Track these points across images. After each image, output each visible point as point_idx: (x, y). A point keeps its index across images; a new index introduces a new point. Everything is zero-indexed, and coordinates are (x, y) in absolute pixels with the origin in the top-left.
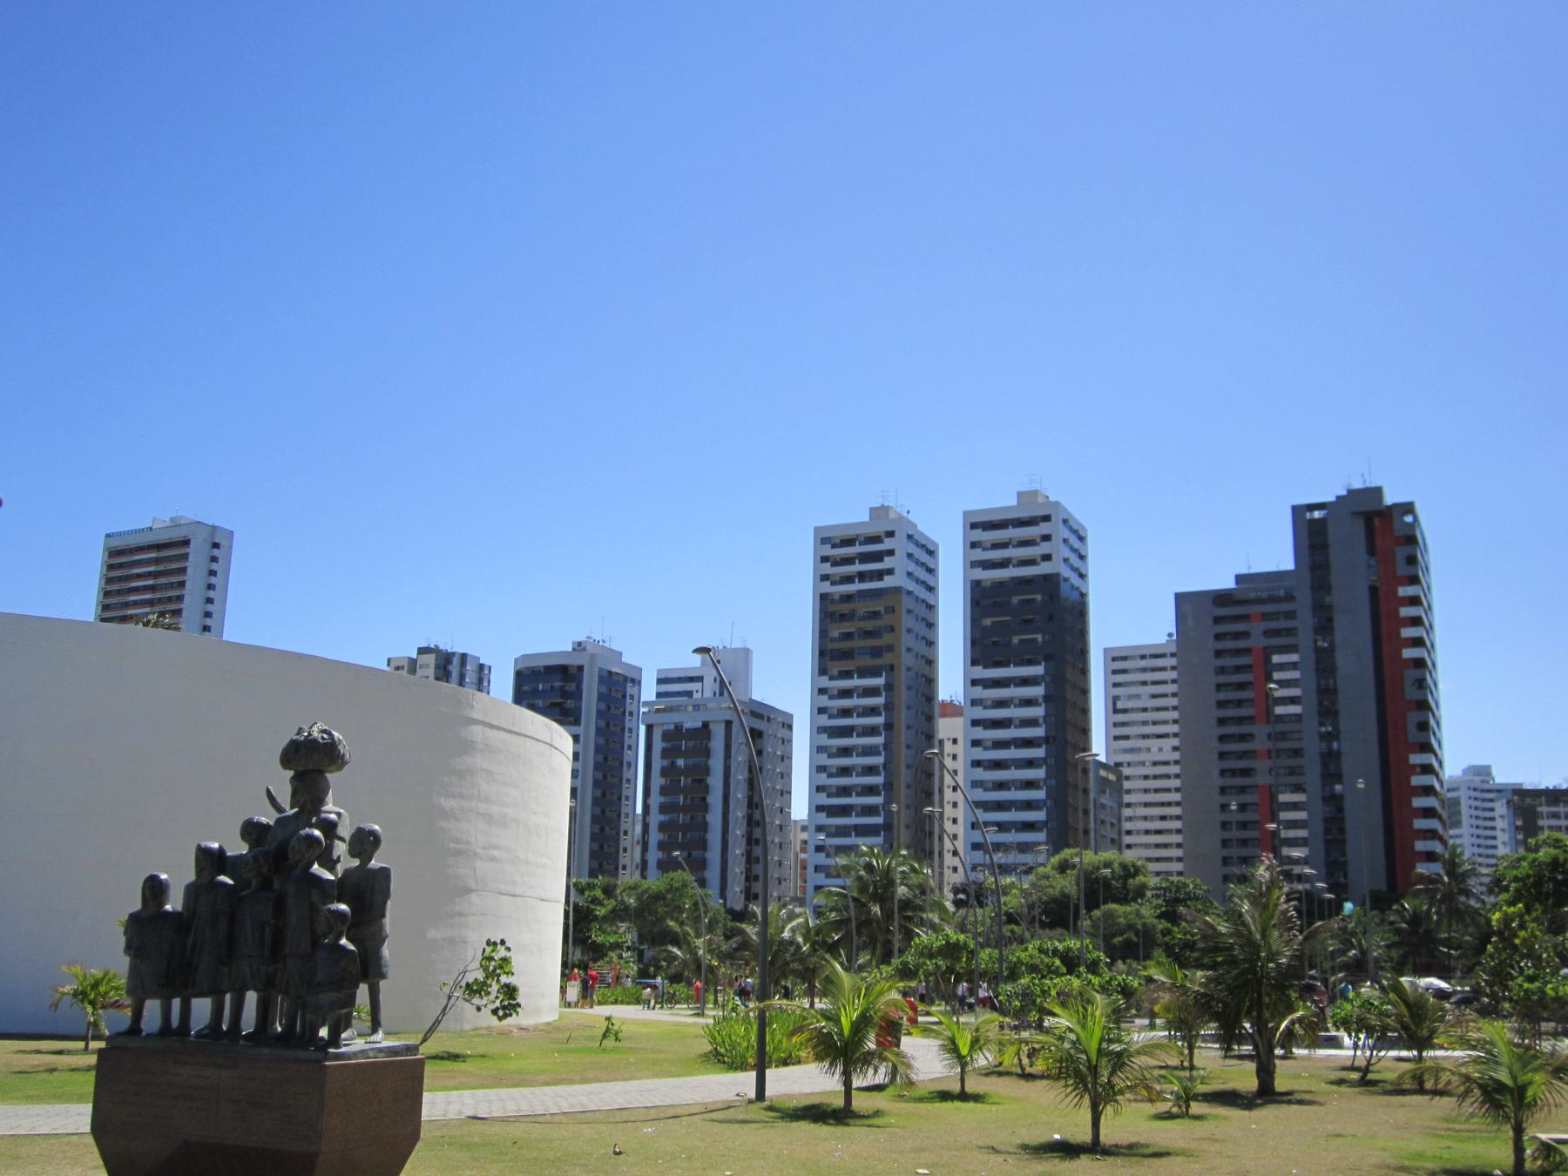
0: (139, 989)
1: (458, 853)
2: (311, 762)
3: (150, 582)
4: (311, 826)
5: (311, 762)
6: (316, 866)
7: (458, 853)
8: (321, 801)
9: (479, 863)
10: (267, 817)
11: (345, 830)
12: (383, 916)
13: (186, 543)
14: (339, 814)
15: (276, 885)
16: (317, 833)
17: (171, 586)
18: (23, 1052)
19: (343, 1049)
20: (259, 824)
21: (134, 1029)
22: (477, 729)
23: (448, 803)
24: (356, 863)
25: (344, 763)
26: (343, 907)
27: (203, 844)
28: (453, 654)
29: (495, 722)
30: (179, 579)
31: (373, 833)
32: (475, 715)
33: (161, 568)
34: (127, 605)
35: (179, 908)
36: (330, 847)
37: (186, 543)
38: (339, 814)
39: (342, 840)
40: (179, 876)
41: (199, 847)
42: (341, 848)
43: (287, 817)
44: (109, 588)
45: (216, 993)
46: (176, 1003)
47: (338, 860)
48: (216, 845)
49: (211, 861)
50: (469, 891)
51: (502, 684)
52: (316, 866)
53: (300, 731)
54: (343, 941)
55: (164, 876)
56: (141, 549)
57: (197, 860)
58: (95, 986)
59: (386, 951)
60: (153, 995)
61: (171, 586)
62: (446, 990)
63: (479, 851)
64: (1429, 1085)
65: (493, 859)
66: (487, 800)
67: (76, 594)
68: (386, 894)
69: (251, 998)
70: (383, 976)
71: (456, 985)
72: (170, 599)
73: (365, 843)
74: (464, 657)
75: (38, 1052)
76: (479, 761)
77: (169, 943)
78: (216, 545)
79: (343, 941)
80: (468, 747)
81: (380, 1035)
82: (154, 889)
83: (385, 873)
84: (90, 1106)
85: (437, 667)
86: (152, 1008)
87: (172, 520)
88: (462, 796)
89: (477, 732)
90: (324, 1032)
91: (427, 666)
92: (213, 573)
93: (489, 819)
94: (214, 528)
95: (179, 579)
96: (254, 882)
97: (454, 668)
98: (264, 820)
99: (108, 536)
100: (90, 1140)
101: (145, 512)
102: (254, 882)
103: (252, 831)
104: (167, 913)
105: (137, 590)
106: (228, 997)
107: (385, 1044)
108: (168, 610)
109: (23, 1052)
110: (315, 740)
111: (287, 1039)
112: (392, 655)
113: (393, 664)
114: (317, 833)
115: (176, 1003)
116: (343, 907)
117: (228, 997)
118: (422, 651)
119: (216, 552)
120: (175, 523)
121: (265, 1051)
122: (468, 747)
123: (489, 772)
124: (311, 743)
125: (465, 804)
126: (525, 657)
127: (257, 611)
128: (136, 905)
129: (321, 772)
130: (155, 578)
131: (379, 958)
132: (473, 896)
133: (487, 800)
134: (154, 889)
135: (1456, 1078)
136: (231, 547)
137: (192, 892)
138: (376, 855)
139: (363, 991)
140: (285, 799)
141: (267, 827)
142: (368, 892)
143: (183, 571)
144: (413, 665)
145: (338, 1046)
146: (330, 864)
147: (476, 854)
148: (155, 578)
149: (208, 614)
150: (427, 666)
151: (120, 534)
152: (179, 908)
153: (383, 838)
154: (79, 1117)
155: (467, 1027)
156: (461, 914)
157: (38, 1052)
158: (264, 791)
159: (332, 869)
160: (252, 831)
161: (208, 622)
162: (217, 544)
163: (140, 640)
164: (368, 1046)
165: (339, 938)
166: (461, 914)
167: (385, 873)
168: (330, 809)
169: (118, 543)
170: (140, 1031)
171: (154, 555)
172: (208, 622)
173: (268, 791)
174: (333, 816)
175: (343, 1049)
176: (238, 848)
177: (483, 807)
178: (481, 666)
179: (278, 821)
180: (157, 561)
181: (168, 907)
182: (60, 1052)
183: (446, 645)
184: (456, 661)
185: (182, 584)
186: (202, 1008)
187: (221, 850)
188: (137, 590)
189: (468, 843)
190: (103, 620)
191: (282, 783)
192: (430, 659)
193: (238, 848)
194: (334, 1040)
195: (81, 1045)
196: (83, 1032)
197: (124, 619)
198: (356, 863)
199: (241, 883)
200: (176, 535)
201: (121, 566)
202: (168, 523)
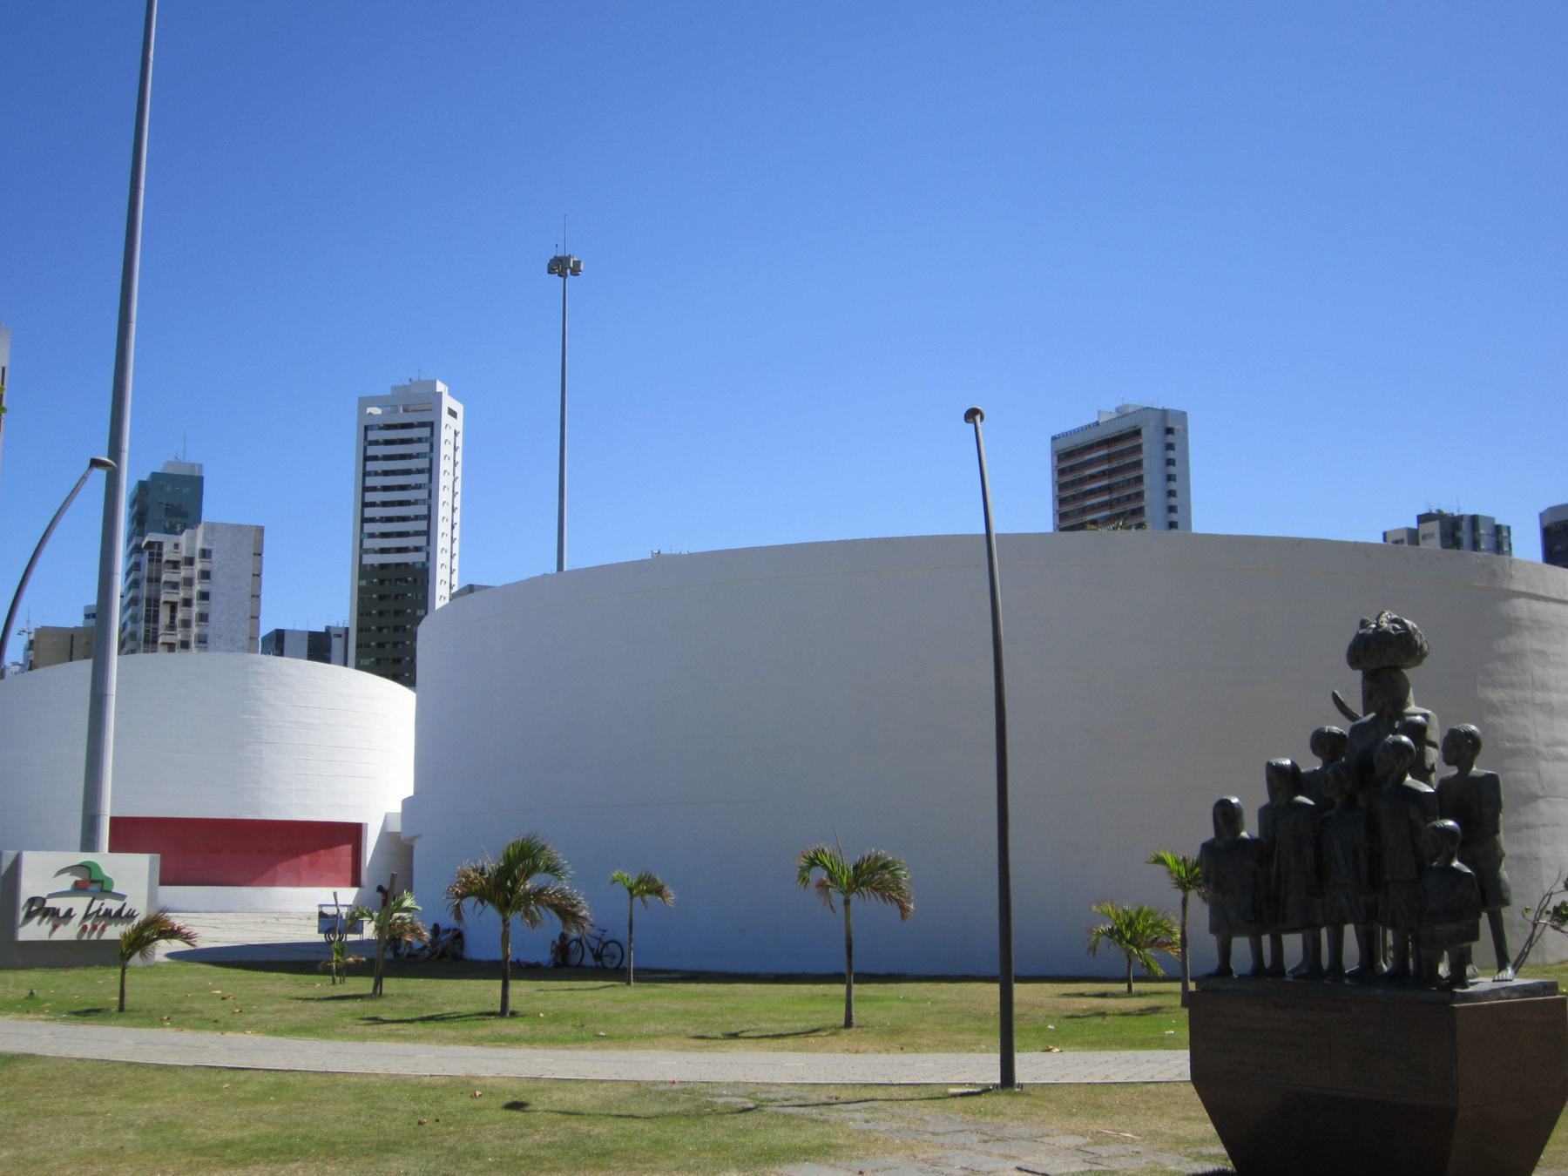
0: (1223, 927)
1: (1515, 753)
2: (1383, 658)
3: (1105, 482)
4: (1395, 732)
5: (1383, 658)
6: (1409, 778)
7: (1515, 753)
8: (1402, 702)
9: (1543, 764)
10: (1338, 726)
11: (1435, 734)
12: (1497, 831)
13: (1137, 433)
14: (1425, 716)
15: (1361, 801)
16: (1405, 739)
17: (1129, 483)
18: (1068, 995)
19: (1471, 989)
20: (1331, 734)
21: (1224, 970)
22: (1520, 603)
23: (1495, 695)
24: (1453, 771)
25: (1423, 655)
26: (1450, 823)
27: (1274, 762)
28: (1461, 517)
29: (1542, 593)
30: (1132, 475)
31: (1470, 734)
32: (1517, 587)
33: (1114, 465)
34: (1084, 511)
35: (1256, 834)
36: (1422, 755)
37: (1137, 433)
38: (1425, 716)
39: (1434, 745)
40: (1250, 798)
41: (1269, 765)
42: (1433, 756)
43: (1364, 724)
44: (1066, 494)
45: (1309, 928)
46: (1266, 940)
47: (1432, 769)
48: (1288, 762)
49: (1283, 780)
50: (1534, 798)
51: (1527, 545)
52: (1409, 778)
53: (1363, 624)
54: (1456, 864)
55: (1235, 800)
56: (1090, 447)
57: (1269, 780)
58: (1130, 925)
59: (1504, 873)
60: (1240, 933)
61: (1129, 483)
62: (1531, 916)
63: (1542, 749)
64: (575, 959)
65: (1561, 758)
66: (1544, 687)
67: (1028, 507)
68: (1497, 805)
69: (1349, 931)
70: (1506, 902)
71: (1541, 911)
72: (1129, 498)
73: (1462, 747)
74: (1474, 520)
75: (1082, 995)
76: (1530, 642)
77: (1246, 872)
78: (1169, 431)
79: (1456, 864)
80: (1511, 626)
81: (1509, 972)
82: (1226, 815)
83: (1492, 782)
84: (1188, 1052)
85: (1443, 535)
86: (1241, 946)
87: (1118, 410)
88: (1512, 685)
89: (1521, 607)
90: (1443, 970)
91: (1432, 536)
92: (1170, 462)
93: (1549, 710)
94: (1164, 412)
95: (1132, 475)
96: (1338, 800)
97: (1465, 534)
98: (1335, 729)
99: (1054, 438)
100: (1192, 1088)
101: (1088, 407)
102: (1338, 800)
103: (1323, 742)
104: (1244, 840)
105: (1092, 493)
106: (1324, 932)
107: (1518, 982)
108: (1129, 513)
109: (1068, 995)
110: (1386, 633)
111: (1399, 976)
112: (1388, 528)
113: (1391, 538)
114: (1405, 739)
115: (1266, 940)
116: (1450, 823)
117: (1324, 932)
118: (1422, 519)
119: (1170, 438)
120: (1122, 413)
121: (1379, 991)
122: (1511, 626)
123: (1542, 653)
124: (1381, 636)
125: (1517, 694)
126: (1553, 510)
127: (1229, 496)
128: (1209, 833)
129: (1397, 669)
130: (1112, 476)
131: (1497, 880)
132: (1542, 805)
133: (1544, 687)
134: (1226, 815)
135: (1174, 953)
136: (1185, 430)
137: (1266, 814)
138: (1477, 760)
139: (1484, 921)
140: (1355, 703)
141: (1341, 736)
142: (1477, 804)
143: (1138, 464)
144: (1413, 536)
145: (1465, 986)
146: (1423, 774)
147: (1538, 753)
148: (1112, 476)
149: (1172, 509)
150: (1432, 536)
151: (1066, 435)
152: (1256, 834)
153: (1482, 739)
154: (1175, 1064)
155: (1550, 960)
156: (1528, 826)
157: (1082, 995)
158: (1328, 696)
159: (1426, 781)
160: (1323, 742)
161: (1174, 517)
162: (1171, 429)
163: (1108, 543)
164: (1497, 985)
165: (1450, 860)
166: (1528, 826)
167: (1492, 782)
168: (1415, 710)
169: (1064, 445)
170: (1230, 972)
171: (1105, 452)
172: (1174, 517)
173: (1335, 697)
174: (1419, 718)
175: (1471, 989)
176: (1311, 764)
177: (1540, 696)
178: (1498, 529)
179: (1353, 729)
180: (1109, 458)
181: (1244, 834)
182: (1104, 995)
183: (1451, 508)
184: (1465, 525)
185: (1139, 479)
186: (1293, 944)
187: (1294, 767)
188: (1092, 493)
189: (1526, 740)
190: (1062, 530)
191: (1351, 684)
192: (1434, 527)
193: (1311, 764)
194: (1459, 977)
195: (1123, 987)
196: (1124, 974)
197: (1082, 527)
198: (1453, 771)
199: (1323, 804)
200: (1126, 425)
201: (1072, 469)
202: (1114, 415)
